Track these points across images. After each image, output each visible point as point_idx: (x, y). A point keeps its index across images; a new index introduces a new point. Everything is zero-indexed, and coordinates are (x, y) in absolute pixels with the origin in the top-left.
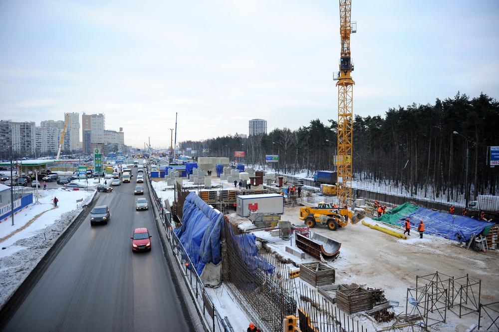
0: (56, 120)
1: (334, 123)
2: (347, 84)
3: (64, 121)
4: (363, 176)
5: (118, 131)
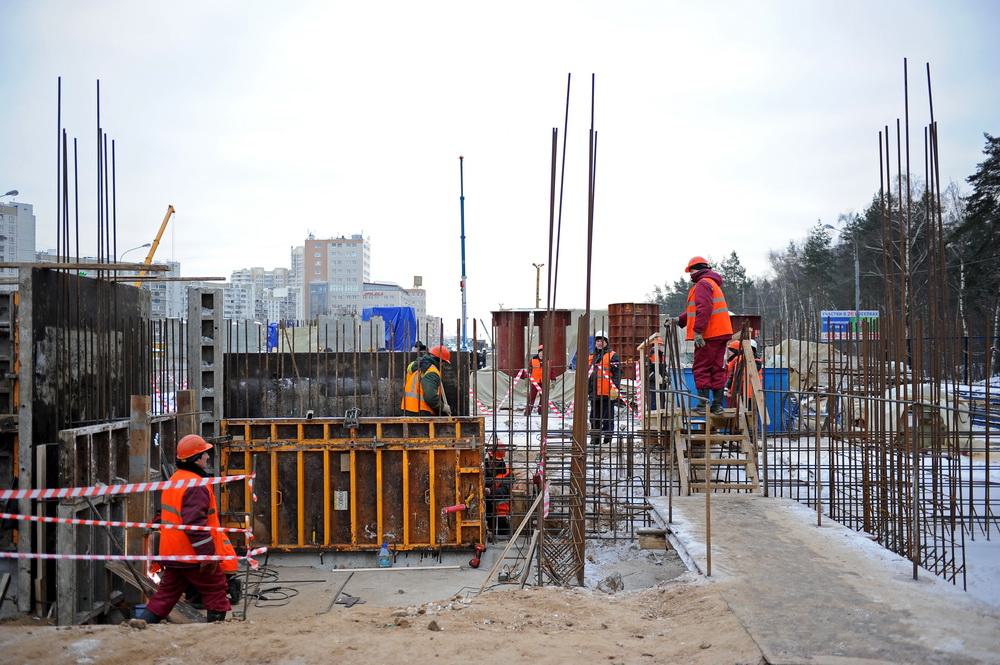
0: (269, 268)
3: (289, 268)
5: (409, 285)
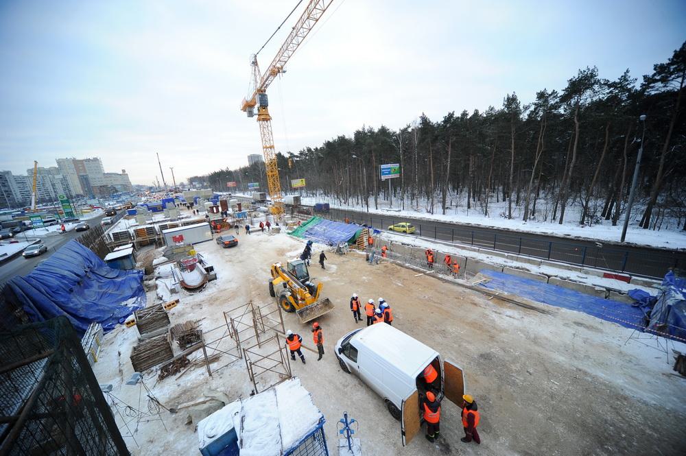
1: (291, 154)
3: (57, 167)
5: (121, 173)
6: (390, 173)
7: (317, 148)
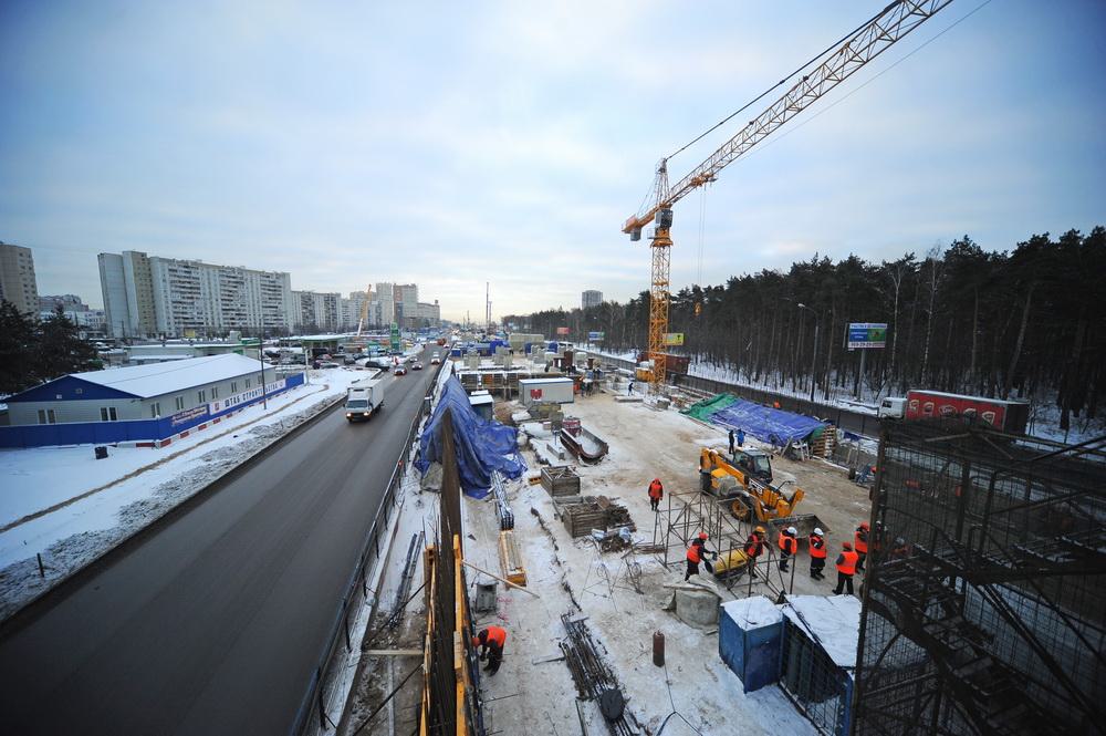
2: (663, 245)
4: (704, 357)
6: (865, 339)
7: (710, 288)
